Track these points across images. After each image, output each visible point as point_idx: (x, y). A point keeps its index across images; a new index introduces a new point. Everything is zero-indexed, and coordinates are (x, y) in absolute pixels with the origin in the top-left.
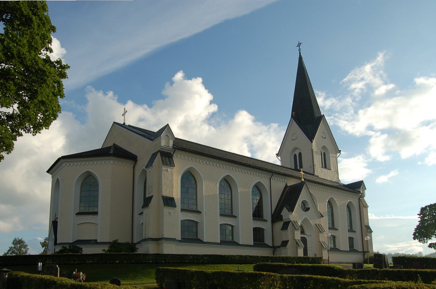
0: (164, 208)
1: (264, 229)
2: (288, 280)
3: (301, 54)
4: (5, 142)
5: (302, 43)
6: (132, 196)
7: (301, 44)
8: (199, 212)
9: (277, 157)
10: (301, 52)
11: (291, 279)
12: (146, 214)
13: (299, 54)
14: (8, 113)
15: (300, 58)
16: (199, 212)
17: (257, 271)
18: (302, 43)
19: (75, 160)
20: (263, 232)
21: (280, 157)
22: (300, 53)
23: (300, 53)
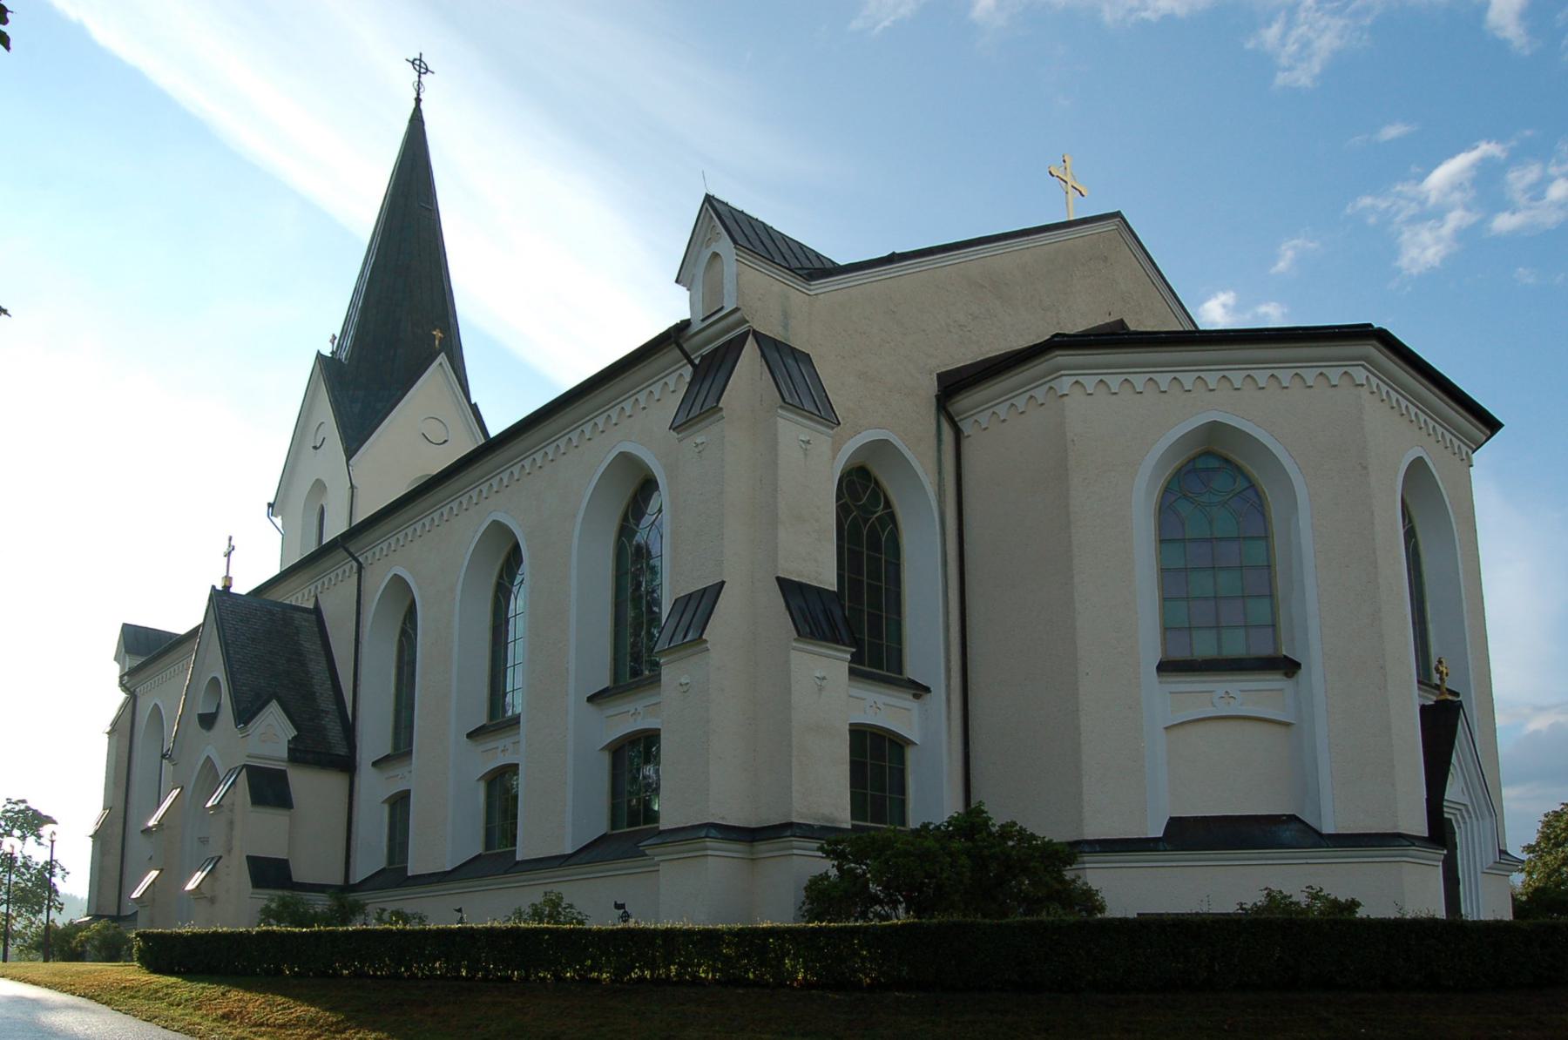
0: (793, 654)
1: (909, 742)
2: (901, 899)
3: (423, 106)
4: (963, 840)
5: (421, 55)
6: (345, 842)
7: (423, 59)
8: (1289, 667)
9: (272, 518)
10: (421, 97)
11: (1022, 895)
12: (700, 448)
13: (413, 105)
14: (59, 904)
15: (417, 122)
16: (1289, 667)
17: (534, 930)
18: (421, 55)
19: (389, 893)
20: (902, 760)
21: (282, 519)
22: (418, 100)
23: (418, 100)
